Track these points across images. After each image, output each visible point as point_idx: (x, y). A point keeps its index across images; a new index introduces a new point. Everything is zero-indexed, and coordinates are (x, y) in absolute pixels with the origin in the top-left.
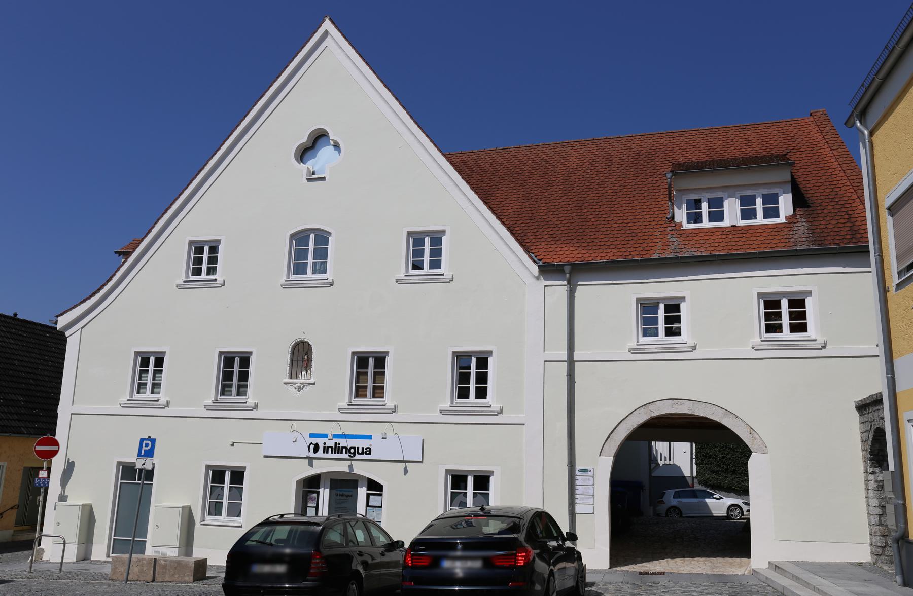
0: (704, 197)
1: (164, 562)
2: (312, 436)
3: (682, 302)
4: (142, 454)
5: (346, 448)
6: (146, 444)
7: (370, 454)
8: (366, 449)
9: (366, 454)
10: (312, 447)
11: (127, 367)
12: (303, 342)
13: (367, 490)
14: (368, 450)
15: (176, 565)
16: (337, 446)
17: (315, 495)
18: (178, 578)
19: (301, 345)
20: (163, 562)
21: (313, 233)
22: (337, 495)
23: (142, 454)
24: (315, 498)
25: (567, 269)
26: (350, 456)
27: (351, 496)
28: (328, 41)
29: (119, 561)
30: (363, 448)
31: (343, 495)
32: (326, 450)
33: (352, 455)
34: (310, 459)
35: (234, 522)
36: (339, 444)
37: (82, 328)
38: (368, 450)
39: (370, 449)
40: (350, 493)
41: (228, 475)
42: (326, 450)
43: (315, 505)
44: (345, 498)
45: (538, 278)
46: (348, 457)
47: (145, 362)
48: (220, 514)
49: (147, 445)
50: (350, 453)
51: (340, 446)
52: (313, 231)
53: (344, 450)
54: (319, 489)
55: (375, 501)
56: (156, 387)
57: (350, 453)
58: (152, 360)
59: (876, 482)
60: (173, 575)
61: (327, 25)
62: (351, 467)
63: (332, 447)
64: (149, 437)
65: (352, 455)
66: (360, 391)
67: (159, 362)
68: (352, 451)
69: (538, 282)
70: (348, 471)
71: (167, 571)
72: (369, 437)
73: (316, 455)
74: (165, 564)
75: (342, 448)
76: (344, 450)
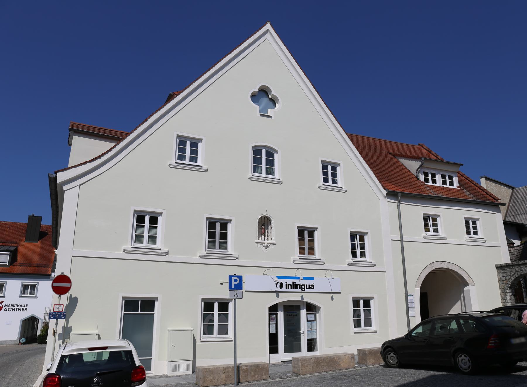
0: (447, 174)
1: (245, 367)
2: (279, 277)
3: (438, 217)
4: (233, 287)
5: (299, 285)
6: (234, 279)
7: (313, 288)
8: (311, 285)
9: (311, 289)
10: (279, 285)
11: (131, 220)
12: (265, 217)
13: (307, 311)
14: (312, 286)
15: (255, 368)
16: (294, 284)
17: (274, 316)
18: (257, 377)
19: (263, 219)
20: (245, 368)
21: (265, 149)
22: (288, 315)
23: (233, 287)
24: (274, 318)
25: (400, 195)
26: (302, 290)
27: (296, 315)
28: (268, 36)
29: (208, 371)
30: (309, 285)
31: (291, 315)
32: (287, 286)
33: (303, 289)
34: (277, 292)
35: (224, 338)
36: (295, 283)
37: (80, 185)
38: (312, 286)
39: (313, 286)
40: (295, 314)
41: (216, 305)
42: (287, 286)
43: (275, 323)
44: (292, 317)
45: (385, 197)
46: (301, 291)
47: (140, 219)
48: (212, 333)
49: (235, 280)
50: (302, 288)
51: (296, 284)
52: (265, 148)
53: (298, 286)
54: (278, 312)
55: (311, 318)
56: (152, 239)
57: (302, 288)
58: (147, 219)
59: (510, 296)
60: (254, 376)
61: (268, 26)
62: (302, 297)
63: (291, 285)
64: (235, 275)
65: (303, 289)
66: (302, 250)
67: (154, 220)
68: (303, 287)
69: (385, 199)
70: (300, 299)
71: (249, 374)
72: (312, 279)
73: (282, 290)
74: (246, 368)
75: (297, 285)
76: (298, 286)
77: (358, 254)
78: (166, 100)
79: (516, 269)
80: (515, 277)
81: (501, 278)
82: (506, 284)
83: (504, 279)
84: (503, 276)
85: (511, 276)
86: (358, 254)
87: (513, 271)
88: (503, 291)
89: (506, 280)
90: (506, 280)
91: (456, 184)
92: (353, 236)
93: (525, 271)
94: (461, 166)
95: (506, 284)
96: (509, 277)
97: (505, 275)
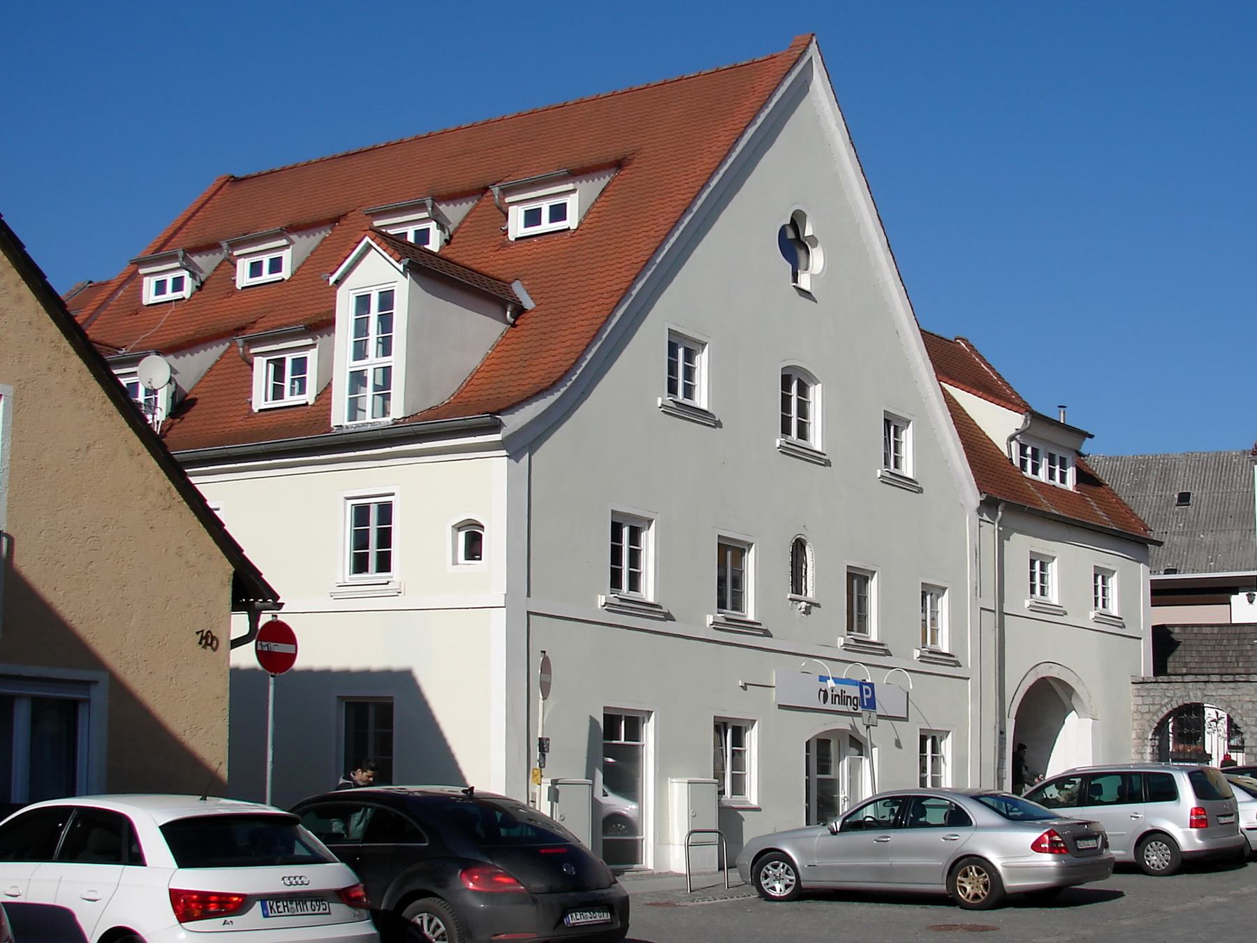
36: (845, 692)
65: (855, 707)
77: (373, 562)
78: (812, 302)
79: (1177, 691)
80: (1170, 709)
81: (1140, 707)
82: (1148, 721)
83: (1145, 709)
84: (1143, 704)
85: (1162, 706)
86: (373, 562)
87: (1169, 695)
88: (1140, 736)
89: (1149, 712)
90: (1149, 712)
91: (1070, 483)
92: (851, 575)
93: (1195, 697)
94: (1087, 439)
95: (1148, 721)
96: (1158, 707)
97: (1149, 700)
